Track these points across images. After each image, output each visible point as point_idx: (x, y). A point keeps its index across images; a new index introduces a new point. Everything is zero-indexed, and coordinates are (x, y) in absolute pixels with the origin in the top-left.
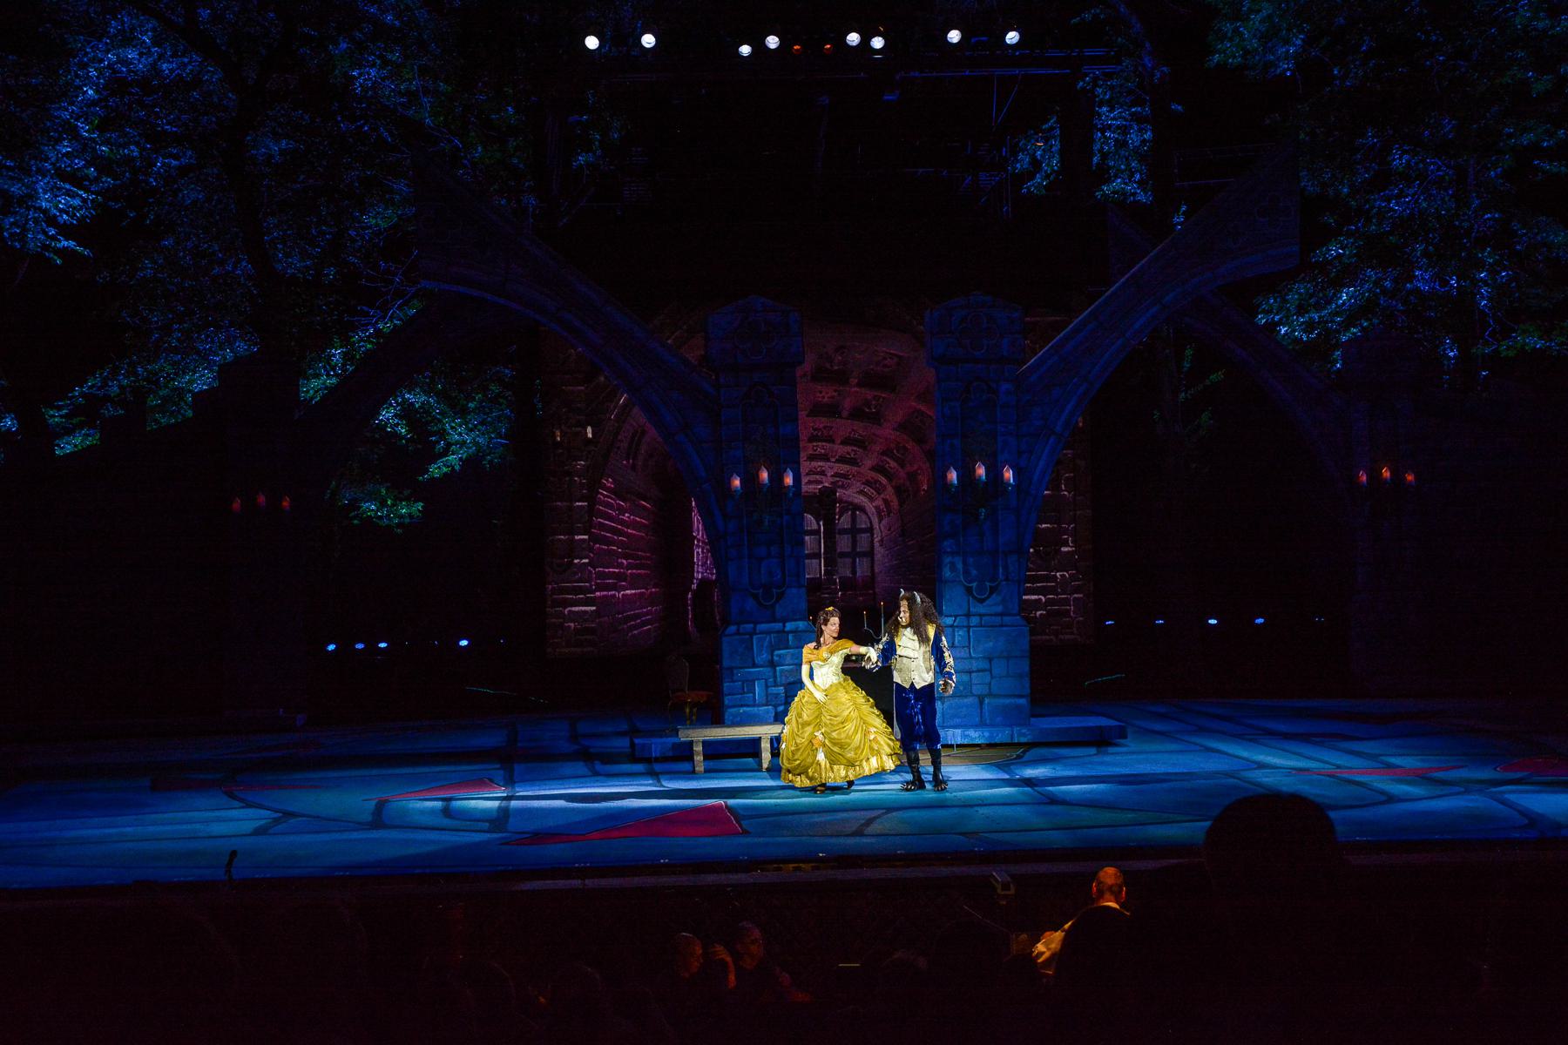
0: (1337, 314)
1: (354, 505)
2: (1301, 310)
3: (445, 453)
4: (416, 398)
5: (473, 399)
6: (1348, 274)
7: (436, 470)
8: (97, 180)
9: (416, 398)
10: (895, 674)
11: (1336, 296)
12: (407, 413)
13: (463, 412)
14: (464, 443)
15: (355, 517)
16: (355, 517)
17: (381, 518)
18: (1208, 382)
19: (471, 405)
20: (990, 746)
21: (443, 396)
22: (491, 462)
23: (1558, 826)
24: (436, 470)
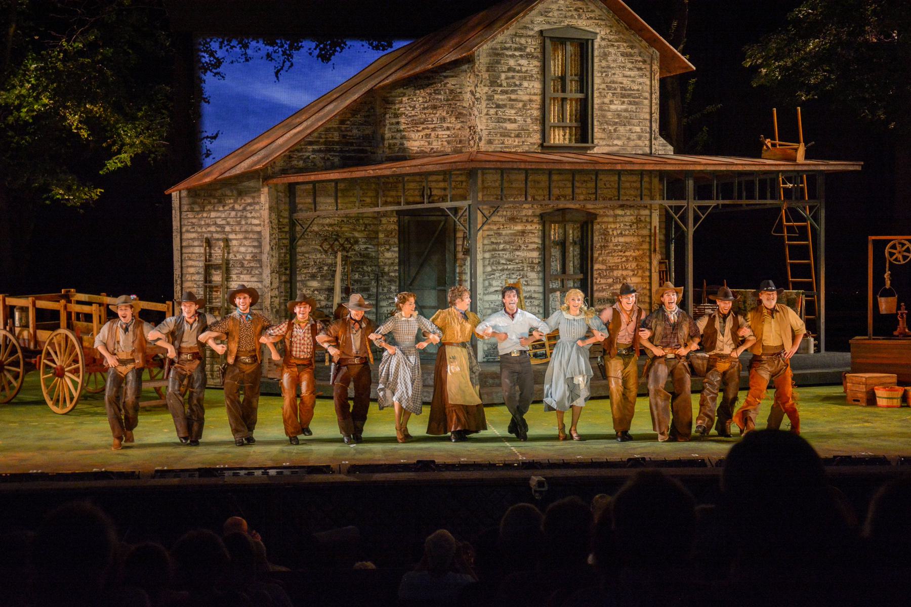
0: (804, 59)
1: (46, 189)
2: (778, 58)
3: (119, 152)
4: (96, 109)
5: (140, 110)
6: (811, 29)
7: (112, 165)
8: (313, 291)
9: (96, 109)
10: (647, 44)
11: (806, 44)
12: (89, 121)
13: (131, 119)
14: (132, 145)
15: (47, 199)
16: (47, 199)
17: (68, 200)
18: (705, 112)
19: (140, 114)
20: (888, 407)
21: (118, 108)
22: (155, 159)
23: (906, 454)
24: (112, 165)
